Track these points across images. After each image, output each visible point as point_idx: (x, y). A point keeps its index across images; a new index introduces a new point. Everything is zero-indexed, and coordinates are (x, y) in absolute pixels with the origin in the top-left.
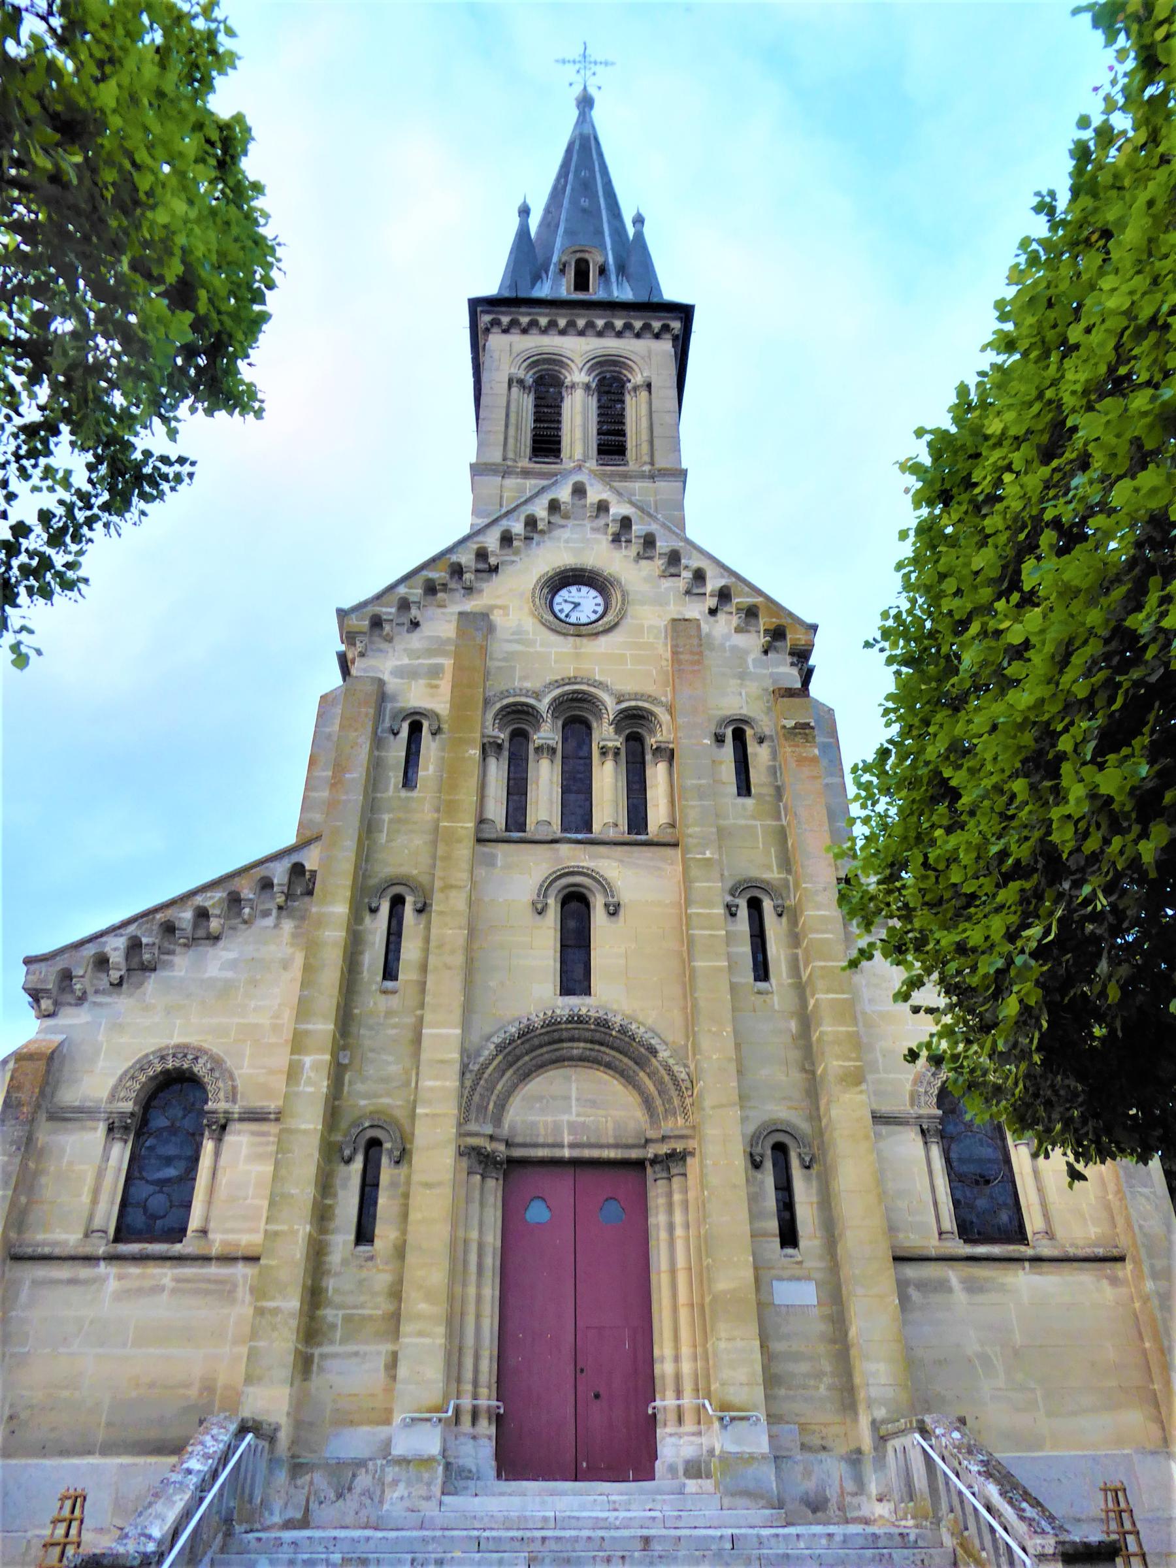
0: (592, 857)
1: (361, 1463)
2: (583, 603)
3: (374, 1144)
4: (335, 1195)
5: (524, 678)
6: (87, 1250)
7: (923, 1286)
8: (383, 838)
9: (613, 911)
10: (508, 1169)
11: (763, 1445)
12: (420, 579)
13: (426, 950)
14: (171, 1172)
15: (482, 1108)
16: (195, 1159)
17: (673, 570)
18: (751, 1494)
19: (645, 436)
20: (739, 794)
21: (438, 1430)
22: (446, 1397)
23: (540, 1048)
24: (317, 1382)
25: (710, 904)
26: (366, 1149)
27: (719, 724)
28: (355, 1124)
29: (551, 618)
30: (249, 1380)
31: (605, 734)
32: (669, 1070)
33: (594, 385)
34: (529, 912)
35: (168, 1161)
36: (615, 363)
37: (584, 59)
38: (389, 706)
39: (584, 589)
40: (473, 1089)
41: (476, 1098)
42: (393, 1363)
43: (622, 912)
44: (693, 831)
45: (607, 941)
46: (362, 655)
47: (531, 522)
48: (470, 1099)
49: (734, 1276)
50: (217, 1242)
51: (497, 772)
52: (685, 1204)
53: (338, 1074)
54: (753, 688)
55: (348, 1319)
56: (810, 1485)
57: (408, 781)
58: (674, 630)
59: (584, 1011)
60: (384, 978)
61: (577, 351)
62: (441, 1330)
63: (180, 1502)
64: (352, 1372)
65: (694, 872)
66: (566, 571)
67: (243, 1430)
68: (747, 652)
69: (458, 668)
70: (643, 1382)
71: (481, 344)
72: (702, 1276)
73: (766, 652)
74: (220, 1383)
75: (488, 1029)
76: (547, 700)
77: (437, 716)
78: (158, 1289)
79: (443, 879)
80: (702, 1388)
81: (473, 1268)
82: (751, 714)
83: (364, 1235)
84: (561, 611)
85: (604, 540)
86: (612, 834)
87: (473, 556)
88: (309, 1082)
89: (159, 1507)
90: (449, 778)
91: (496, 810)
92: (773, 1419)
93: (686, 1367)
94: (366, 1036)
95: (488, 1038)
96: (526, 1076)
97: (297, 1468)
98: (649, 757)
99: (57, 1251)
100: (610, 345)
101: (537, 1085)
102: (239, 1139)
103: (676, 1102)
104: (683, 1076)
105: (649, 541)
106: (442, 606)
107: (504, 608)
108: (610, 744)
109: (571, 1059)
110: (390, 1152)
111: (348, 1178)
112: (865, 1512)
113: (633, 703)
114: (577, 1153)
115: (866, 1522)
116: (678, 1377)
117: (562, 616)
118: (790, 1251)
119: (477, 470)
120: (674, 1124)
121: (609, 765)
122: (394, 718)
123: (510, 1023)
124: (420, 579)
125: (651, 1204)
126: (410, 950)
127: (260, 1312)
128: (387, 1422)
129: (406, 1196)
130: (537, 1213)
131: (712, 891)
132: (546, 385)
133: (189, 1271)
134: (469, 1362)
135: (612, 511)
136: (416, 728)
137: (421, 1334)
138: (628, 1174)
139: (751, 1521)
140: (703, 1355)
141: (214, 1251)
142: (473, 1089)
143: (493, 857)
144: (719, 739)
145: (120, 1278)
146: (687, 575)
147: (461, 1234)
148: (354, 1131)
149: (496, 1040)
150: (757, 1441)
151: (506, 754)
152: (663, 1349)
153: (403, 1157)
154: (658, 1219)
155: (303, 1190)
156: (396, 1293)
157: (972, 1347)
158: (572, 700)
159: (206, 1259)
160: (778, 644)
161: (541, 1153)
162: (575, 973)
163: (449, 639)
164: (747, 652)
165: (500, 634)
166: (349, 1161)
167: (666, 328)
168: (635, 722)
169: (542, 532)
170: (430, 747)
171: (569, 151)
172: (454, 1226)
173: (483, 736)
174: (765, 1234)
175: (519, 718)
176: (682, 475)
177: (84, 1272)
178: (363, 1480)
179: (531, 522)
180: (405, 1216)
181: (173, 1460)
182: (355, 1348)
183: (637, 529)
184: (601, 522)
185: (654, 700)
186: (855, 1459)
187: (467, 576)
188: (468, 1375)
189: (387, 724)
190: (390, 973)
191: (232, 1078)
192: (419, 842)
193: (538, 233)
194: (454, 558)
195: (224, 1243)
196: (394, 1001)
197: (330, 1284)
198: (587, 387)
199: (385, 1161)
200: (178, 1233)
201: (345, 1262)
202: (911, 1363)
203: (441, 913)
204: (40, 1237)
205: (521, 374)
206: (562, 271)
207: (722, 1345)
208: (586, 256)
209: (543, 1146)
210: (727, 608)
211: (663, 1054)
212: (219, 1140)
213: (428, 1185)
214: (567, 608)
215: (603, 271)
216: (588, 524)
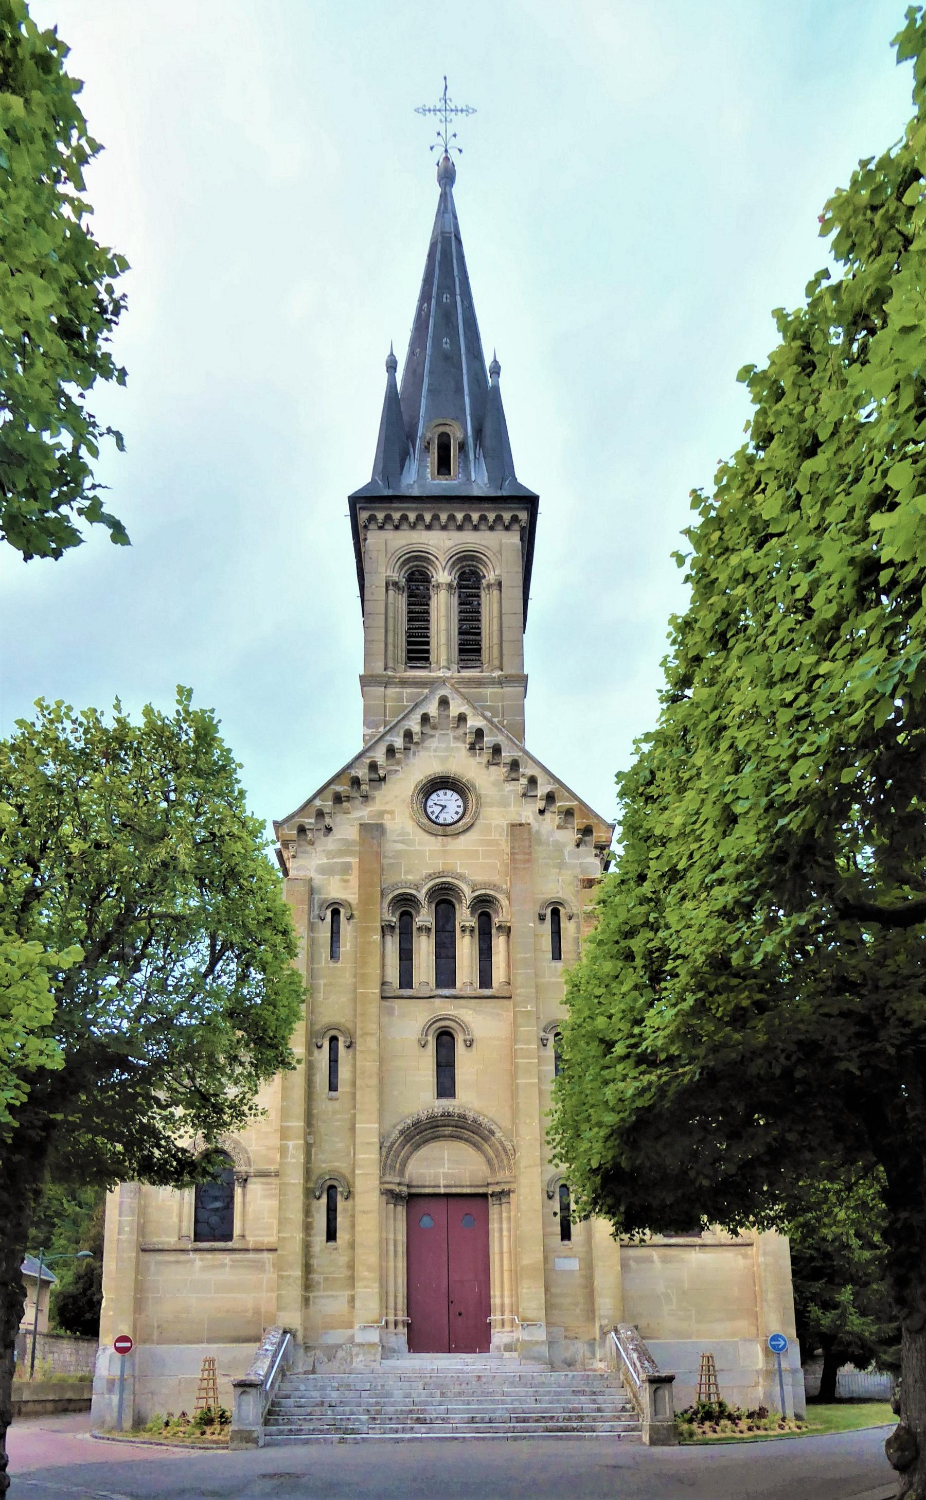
0: (456, 1008)
1: (339, 1346)
2: (448, 804)
3: (332, 1188)
4: (313, 1217)
5: (406, 873)
6: (182, 1247)
7: (638, 1260)
8: (320, 997)
9: (469, 1044)
10: (410, 1200)
11: (543, 1337)
12: (329, 793)
13: (354, 1072)
14: (218, 1204)
15: (393, 1167)
16: (232, 1197)
17: (514, 775)
18: (537, 1359)
19: (496, 640)
20: (553, 959)
21: (378, 1331)
22: (381, 1316)
23: (425, 1131)
24: (312, 1308)
25: (528, 1042)
26: (328, 1193)
27: (542, 907)
28: (319, 1177)
29: (426, 821)
30: (279, 1309)
31: (464, 916)
32: (501, 1143)
33: (455, 583)
34: (416, 1046)
35: (216, 1199)
36: (473, 558)
37: (445, 108)
38: (316, 897)
39: (449, 793)
40: (387, 1157)
41: (389, 1162)
42: (352, 1299)
43: (474, 1044)
44: (521, 991)
45: (466, 1064)
46: (294, 857)
47: (408, 735)
48: (385, 1165)
49: (533, 1256)
50: (251, 1241)
51: (393, 945)
52: (509, 1218)
53: (308, 1149)
54: (567, 875)
55: (326, 1279)
56: (568, 1355)
57: (334, 955)
58: (512, 835)
59: (451, 1109)
60: (330, 1090)
61: (441, 544)
62: (377, 1285)
63: (267, 1362)
64: (332, 1304)
65: (520, 1020)
66: (435, 778)
67: (285, 1332)
68: (564, 845)
69: (363, 871)
70: (485, 1307)
71: (362, 537)
72: (515, 1256)
73: (578, 846)
74: (263, 1310)
75: (394, 1121)
76: (424, 891)
77: (350, 905)
78: (223, 1266)
79: (362, 1029)
80: (514, 1310)
81: (392, 1253)
82: (565, 897)
83: (331, 1235)
84: (433, 812)
85: (463, 747)
86: (468, 992)
87: (367, 771)
88: (293, 1157)
89: (259, 1364)
90: (361, 959)
91: (393, 975)
92: (549, 1324)
93: (507, 1301)
94: (321, 1126)
95: (394, 1126)
96: (417, 1147)
97: (307, 1348)
98: (494, 931)
99: (166, 1247)
100: (469, 539)
101: (424, 1151)
102: (255, 1187)
103: (505, 1162)
104: (510, 1147)
105: (497, 750)
106: (347, 812)
107: (391, 812)
108: (467, 924)
109: (444, 1136)
110: (342, 1193)
111: (319, 1207)
112: (594, 1367)
113: (483, 892)
114: (448, 1191)
115: (595, 1370)
116: (502, 1305)
117: (433, 817)
118: (566, 1242)
119: (366, 681)
120: (501, 1176)
121: (467, 939)
122: (320, 907)
123: (407, 1117)
124: (329, 793)
125: (491, 1217)
126: (344, 1072)
127: (281, 1277)
128: (352, 1327)
129: (353, 1216)
130: (426, 1222)
131: (531, 1030)
132: (416, 580)
133: (238, 1256)
134: (391, 1299)
135: (469, 723)
136: (336, 913)
137: (366, 1287)
138: (476, 1203)
139: (532, 1369)
140: (515, 1294)
141: (251, 1246)
142: (387, 1157)
143: (393, 1008)
144: (542, 918)
145: (202, 1260)
146: (524, 781)
147: (384, 1235)
148: (320, 1182)
149: (400, 1128)
150: (541, 1335)
151: (397, 931)
152: (495, 1292)
153: (349, 1195)
154: (494, 1226)
155: (296, 1214)
156: (351, 1266)
157: (661, 1288)
158: (441, 889)
159: (247, 1250)
160: (587, 838)
161: (427, 1191)
162: (446, 1086)
163: (354, 841)
164: (564, 845)
165: (391, 836)
166: (319, 1198)
167: (515, 519)
168: (484, 906)
169: (417, 743)
170: (346, 929)
171: (433, 246)
172: (380, 1232)
173: (382, 921)
174: (552, 1234)
175: (405, 904)
176: (523, 680)
177: (182, 1257)
178: (341, 1354)
179: (408, 735)
180: (353, 1226)
181: (258, 1344)
182: (330, 1293)
183: (488, 740)
184: (461, 732)
185: (496, 887)
186: (591, 1344)
187: (363, 787)
188: (391, 1304)
189: (316, 912)
190: (333, 1087)
191: (246, 1152)
192: (344, 999)
193: (404, 386)
194: (353, 773)
195: (255, 1242)
196: (336, 1105)
197: (315, 1262)
198: (450, 586)
199: (339, 1198)
200: (228, 1237)
201: (321, 1251)
202: (624, 1299)
203: (362, 1052)
204: (155, 1240)
205: (395, 577)
206: (427, 448)
207: (525, 1291)
208: (446, 429)
209: (429, 1187)
210: (552, 809)
211: (498, 1134)
212: (244, 1187)
213: (364, 1212)
214: (437, 809)
215: (462, 446)
216: (451, 734)
